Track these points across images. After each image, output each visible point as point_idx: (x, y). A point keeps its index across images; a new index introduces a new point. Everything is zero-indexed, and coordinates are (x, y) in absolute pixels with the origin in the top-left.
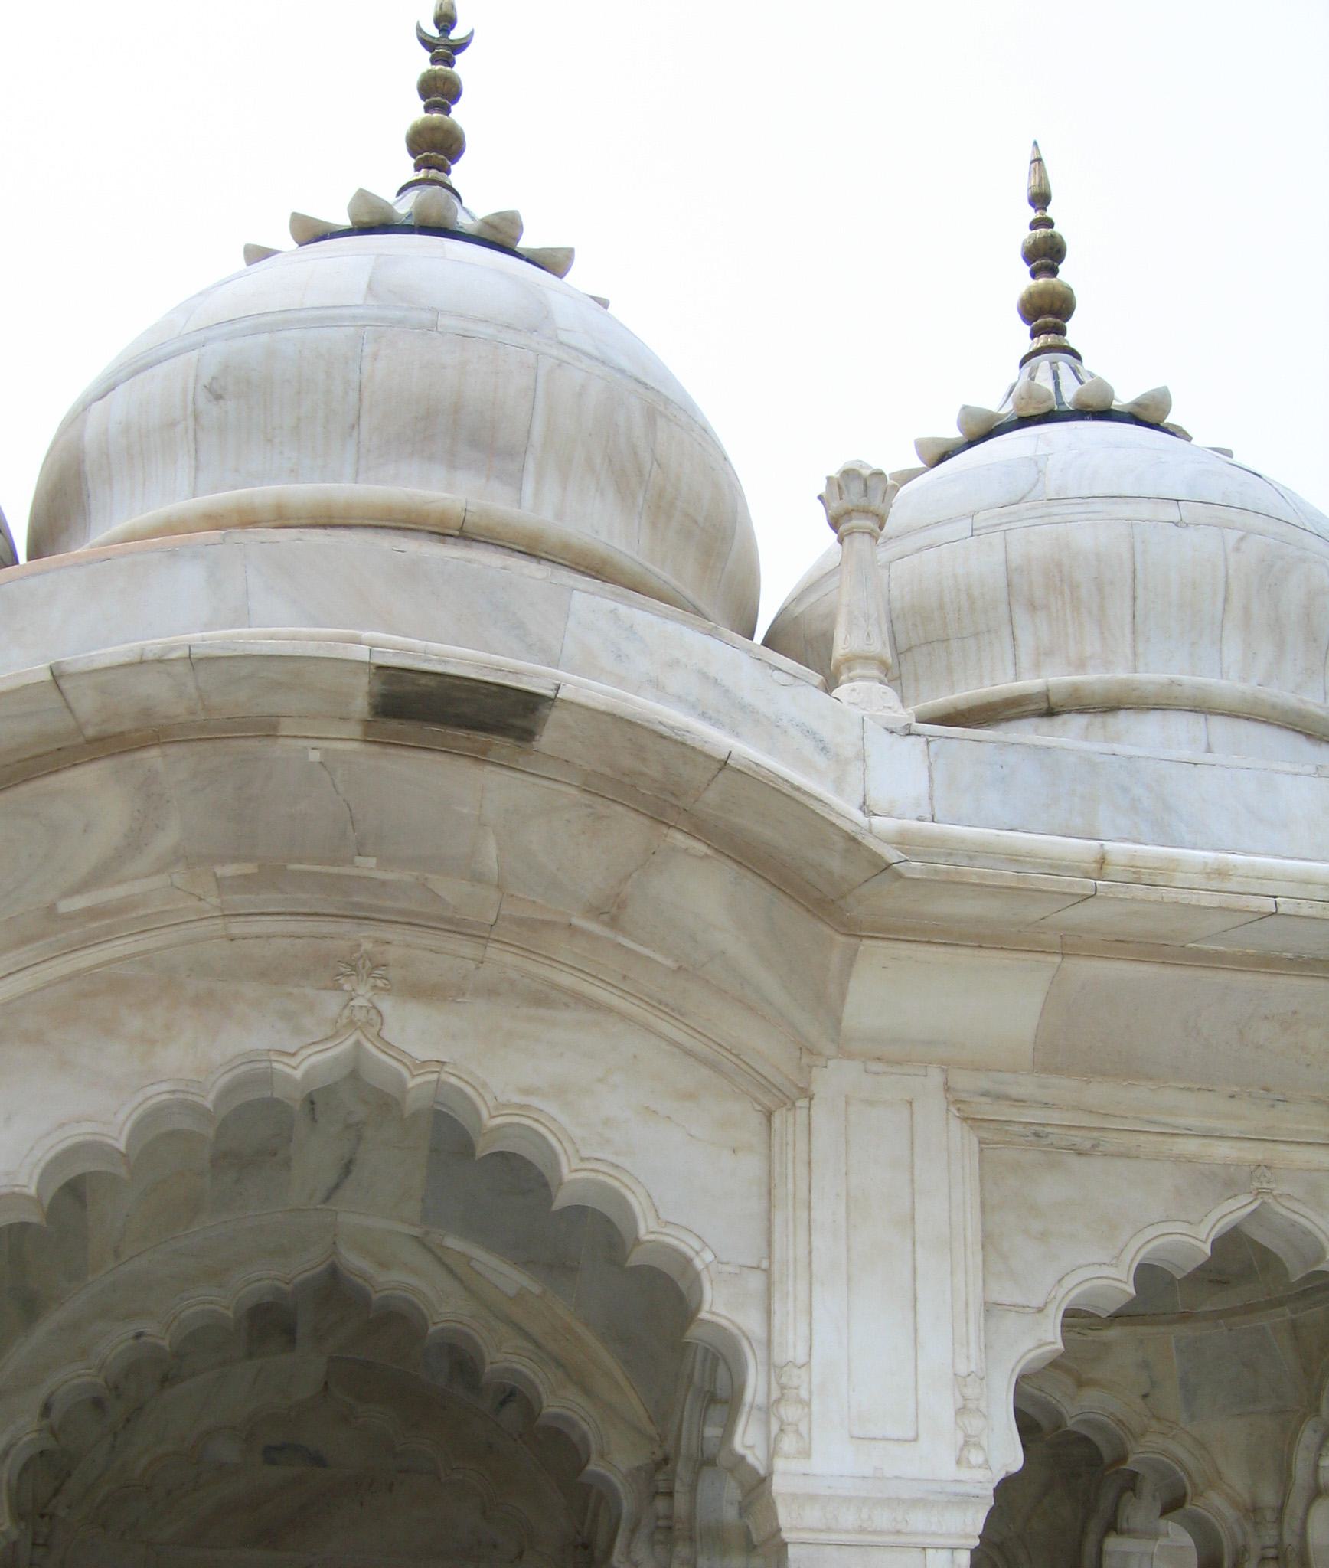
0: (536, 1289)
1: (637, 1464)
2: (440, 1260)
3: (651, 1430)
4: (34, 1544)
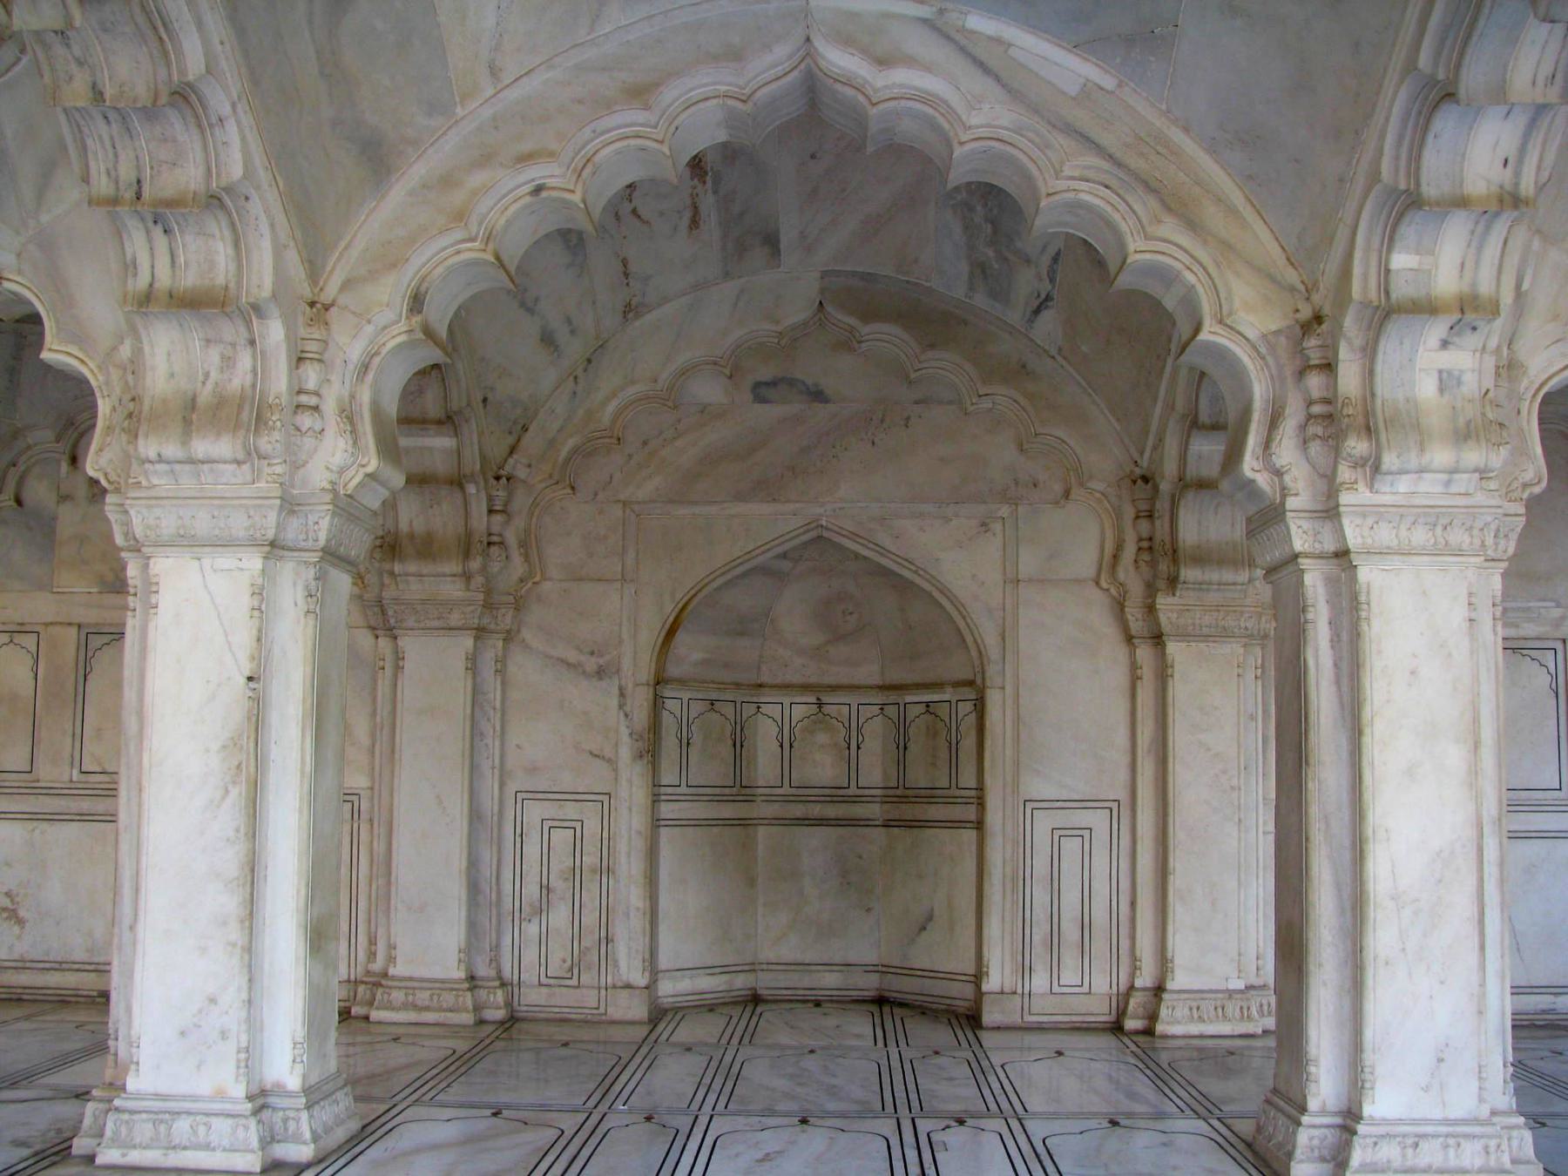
0: (1108, 82)
1: (1274, 328)
2: (963, 50)
3: (1292, 277)
4: (491, 511)
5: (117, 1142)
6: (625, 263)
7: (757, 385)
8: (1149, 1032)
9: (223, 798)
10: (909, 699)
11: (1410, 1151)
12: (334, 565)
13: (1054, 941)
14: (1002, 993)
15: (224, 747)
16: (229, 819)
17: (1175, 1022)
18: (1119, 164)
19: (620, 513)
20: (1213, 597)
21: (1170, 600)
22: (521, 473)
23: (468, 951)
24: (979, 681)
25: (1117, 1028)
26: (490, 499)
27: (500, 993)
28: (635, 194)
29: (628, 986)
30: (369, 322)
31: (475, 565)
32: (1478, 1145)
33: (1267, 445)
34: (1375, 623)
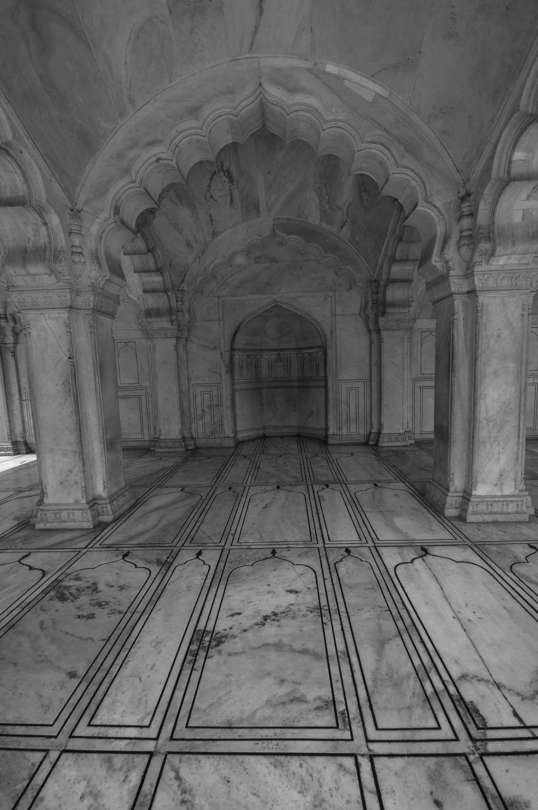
0: (385, 93)
3: (458, 177)
4: (177, 301)
5: (42, 521)
6: (210, 216)
7: (255, 258)
8: (376, 445)
9: (65, 402)
10: (304, 352)
11: (490, 507)
12: (101, 315)
13: (348, 420)
14: (333, 435)
15: (63, 383)
16: (68, 409)
17: (384, 443)
18: (388, 132)
19: (217, 300)
20: (396, 317)
21: (383, 319)
22: (186, 289)
23: (181, 431)
24: (325, 346)
25: (366, 444)
26: (177, 297)
27: (192, 441)
28: (211, 189)
29: (228, 437)
30: (97, 218)
31: (174, 317)
32: (514, 505)
33: (442, 250)
34: (484, 318)
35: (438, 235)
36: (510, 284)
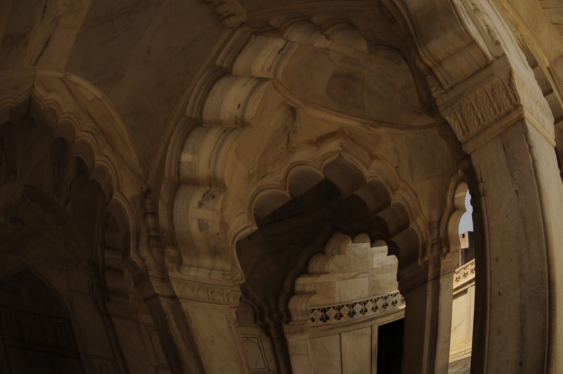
0: (100, 96)
35: (131, 229)
36: (208, 297)
